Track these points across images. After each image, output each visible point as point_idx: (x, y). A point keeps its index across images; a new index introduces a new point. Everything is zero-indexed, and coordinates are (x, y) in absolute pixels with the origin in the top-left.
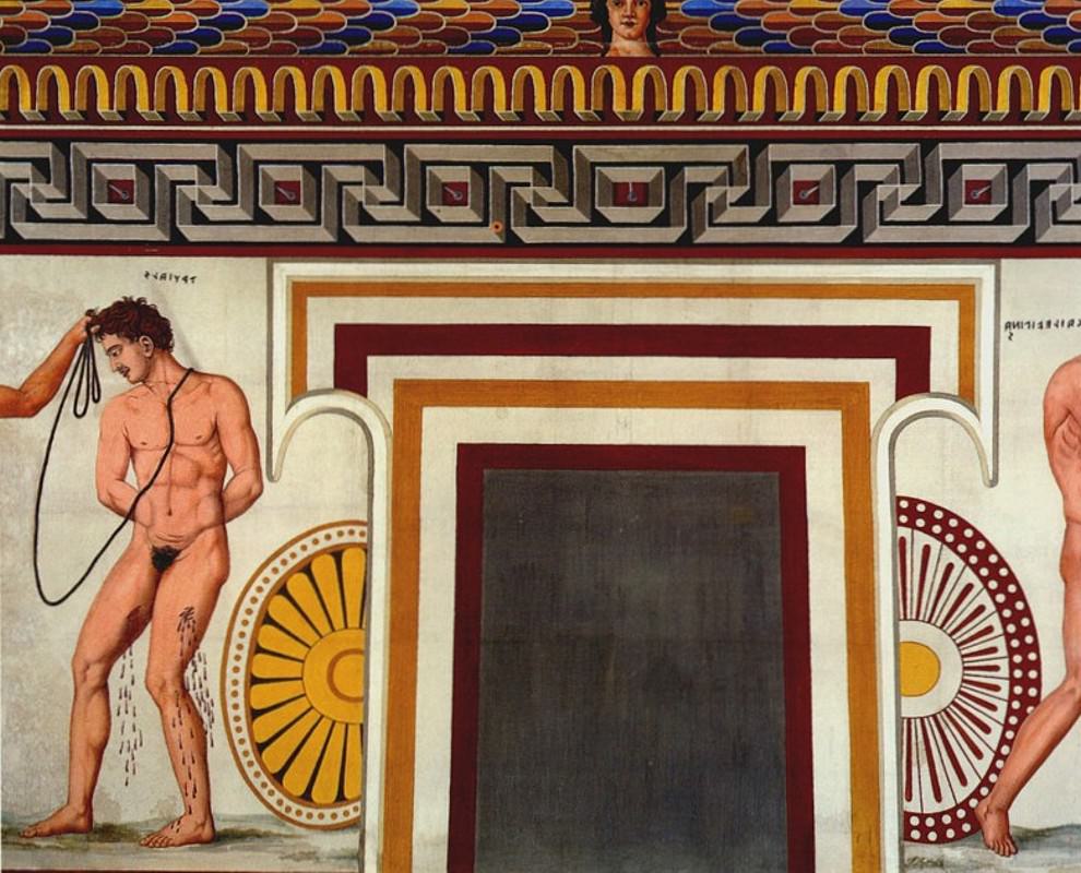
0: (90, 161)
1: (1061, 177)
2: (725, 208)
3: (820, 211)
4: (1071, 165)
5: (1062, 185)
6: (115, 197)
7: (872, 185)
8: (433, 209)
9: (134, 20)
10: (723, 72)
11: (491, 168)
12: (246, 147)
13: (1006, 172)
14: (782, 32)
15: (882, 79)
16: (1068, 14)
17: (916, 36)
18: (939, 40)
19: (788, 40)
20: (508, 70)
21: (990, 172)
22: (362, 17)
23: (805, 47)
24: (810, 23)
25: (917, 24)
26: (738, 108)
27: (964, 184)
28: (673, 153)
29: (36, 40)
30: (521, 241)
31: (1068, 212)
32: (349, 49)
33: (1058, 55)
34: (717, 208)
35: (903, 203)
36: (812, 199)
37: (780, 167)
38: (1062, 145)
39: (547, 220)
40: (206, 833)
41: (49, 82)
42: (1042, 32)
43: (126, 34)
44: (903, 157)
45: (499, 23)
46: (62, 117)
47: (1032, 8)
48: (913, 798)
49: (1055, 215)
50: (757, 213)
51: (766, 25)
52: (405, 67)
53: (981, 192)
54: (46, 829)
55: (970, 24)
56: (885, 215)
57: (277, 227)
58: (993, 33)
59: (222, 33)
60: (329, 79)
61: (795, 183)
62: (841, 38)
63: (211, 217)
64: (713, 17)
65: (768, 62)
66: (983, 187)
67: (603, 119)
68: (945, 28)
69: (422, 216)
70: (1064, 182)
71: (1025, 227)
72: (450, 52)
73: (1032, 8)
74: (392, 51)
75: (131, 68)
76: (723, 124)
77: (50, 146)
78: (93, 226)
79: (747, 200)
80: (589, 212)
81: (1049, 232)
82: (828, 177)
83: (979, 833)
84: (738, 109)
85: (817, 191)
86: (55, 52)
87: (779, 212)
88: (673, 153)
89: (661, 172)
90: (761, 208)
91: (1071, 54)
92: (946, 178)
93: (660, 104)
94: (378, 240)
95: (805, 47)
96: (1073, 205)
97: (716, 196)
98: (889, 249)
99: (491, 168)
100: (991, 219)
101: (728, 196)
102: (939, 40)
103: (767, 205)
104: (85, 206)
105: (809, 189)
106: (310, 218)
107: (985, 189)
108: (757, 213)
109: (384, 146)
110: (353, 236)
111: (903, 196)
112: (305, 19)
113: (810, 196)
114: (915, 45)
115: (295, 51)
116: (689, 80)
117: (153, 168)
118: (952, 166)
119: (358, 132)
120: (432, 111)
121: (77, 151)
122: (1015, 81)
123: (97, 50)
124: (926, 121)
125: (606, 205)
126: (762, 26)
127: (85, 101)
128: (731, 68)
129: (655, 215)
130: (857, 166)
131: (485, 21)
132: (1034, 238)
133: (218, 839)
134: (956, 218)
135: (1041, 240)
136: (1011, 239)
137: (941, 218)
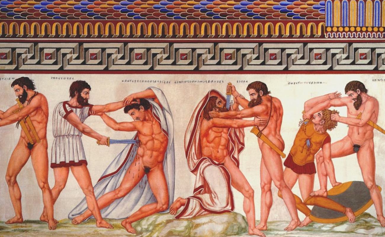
1: (250, 53)
2: (252, 61)
3: (97, 62)
4: (73, 49)
5: (115, 55)
6: (95, 58)
7: (156, 54)
10: (172, 24)
13: (56, 51)
14: (179, 14)
15: (12, 25)
16: (133, 9)
17: (253, 15)
18: (153, 15)
19: (73, 15)
21: (142, 51)
23: (210, 17)
24: (185, 11)
25: (214, 11)
26: (272, 34)
27: (90, 55)
29: (3, 13)
31: (44, 62)
33: (10, 19)
34: (24, 60)
35: (164, 59)
37: (42, 49)
38: (286, 44)
40: (265, 228)
42: (206, 14)
44: (253, 47)
47: (162, 7)
49: (204, 63)
50: (81, 61)
51: (254, 12)
53: (185, 57)
54: (11, 222)
55: (227, 12)
56: (160, 62)
58: (233, 14)
61: (181, 54)
62: (100, 15)
64: (121, 9)
65: (120, 21)
66: (4, 55)
68: (168, 13)
70: (206, 54)
71: (196, 66)
73: (162, 7)
76: (98, 38)
79: (78, 58)
81: (22, 67)
82: (369, 52)
84: (282, 34)
85: (187, 56)
87: (177, 62)
89: (100, 51)
90: (81, 60)
91: (293, 20)
92: (310, 52)
93: (293, 33)
94: (31, 69)
95: (210, 17)
96: (28, 60)
97: (339, 57)
98: (360, 71)
100: (259, 64)
101: (298, 57)
102: (153, 15)
103: (190, 59)
105: (94, 55)
107: (186, 56)
108: (81, 61)
111: (74, 57)
113: (274, 58)
114: (128, 13)
116: (131, 26)
118: (132, 50)
119: (357, 40)
122: (301, 27)
124: (215, 37)
126: (53, 12)
128: (153, 23)
129: (82, 62)
130: (90, 49)
132: (108, 69)
133: (22, 222)
134: (42, 63)
135: (155, 69)
136: (57, 69)
137: (263, 64)
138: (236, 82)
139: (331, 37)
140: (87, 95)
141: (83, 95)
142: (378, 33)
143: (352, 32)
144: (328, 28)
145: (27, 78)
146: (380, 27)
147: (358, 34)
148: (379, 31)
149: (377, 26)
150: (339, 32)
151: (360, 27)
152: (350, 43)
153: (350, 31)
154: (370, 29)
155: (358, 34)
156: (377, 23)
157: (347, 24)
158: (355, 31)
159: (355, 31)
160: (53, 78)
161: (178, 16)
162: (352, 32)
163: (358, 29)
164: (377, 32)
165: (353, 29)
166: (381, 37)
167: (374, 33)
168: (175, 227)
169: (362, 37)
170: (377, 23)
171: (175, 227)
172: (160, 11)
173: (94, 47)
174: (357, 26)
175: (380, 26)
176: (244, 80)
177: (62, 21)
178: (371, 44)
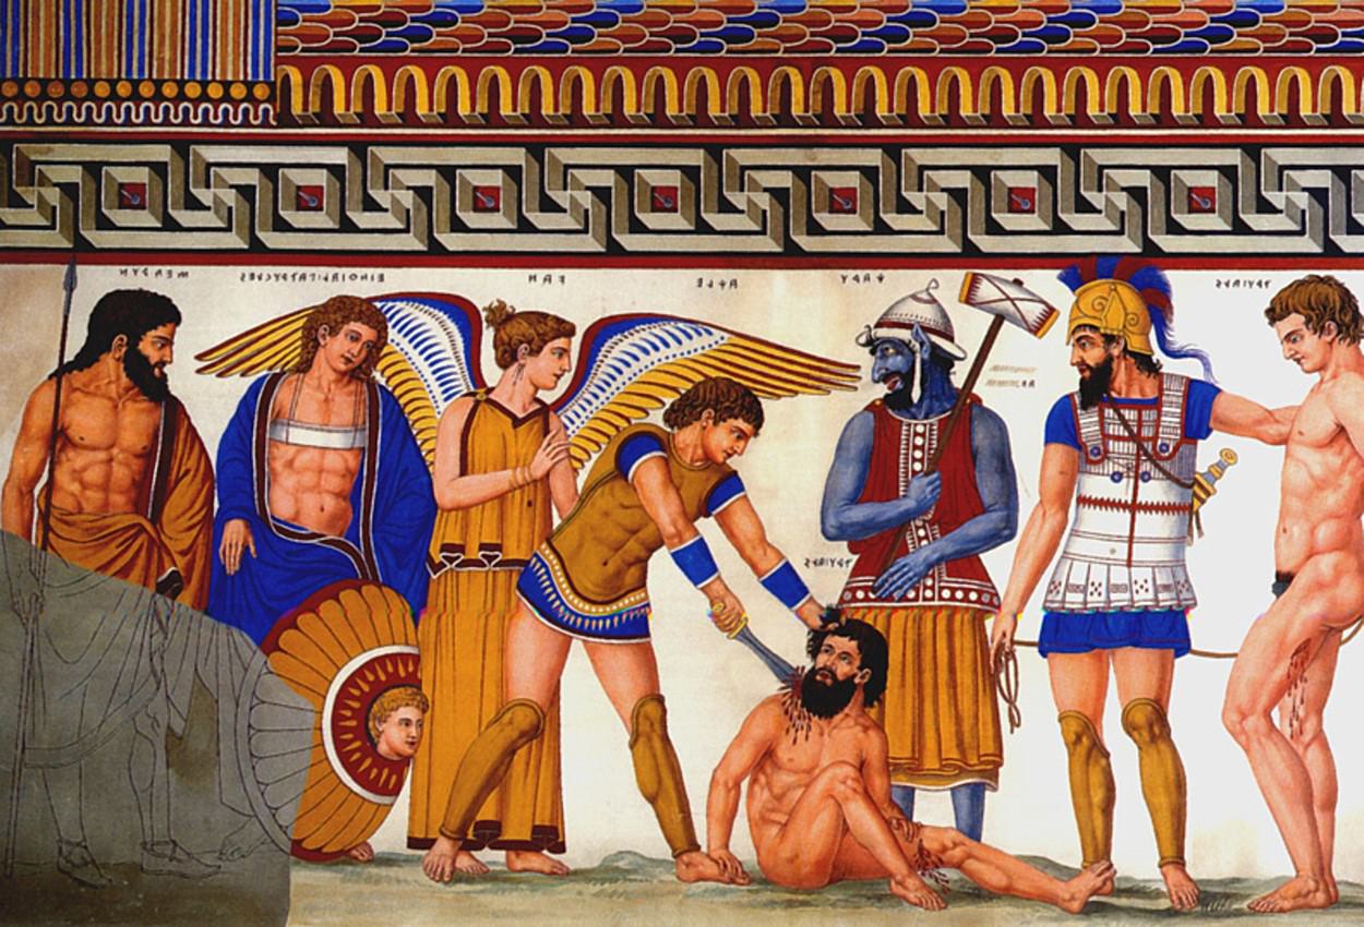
0: (1282, 168)
6: (1015, 206)
8: (1064, 217)
9: (1132, 18)
11: (813, 173)
12: (1270, 151)
20: (1059, 71)
22: (375, 14)
28: (796, 157)
30: (800, 248)
32: (887, 47)
36: (836, 206)
38: (851, 151)
39: (718, 228)
41: (1120, 86)
43: (967, 32)
45: (889, 20)
46: (1301, 119)
48: (402, 793)
52: (615, 68)
57: (539, 235)
59: (1071, 31)
60: (1039, 82)
63: (471, 225)
67: (612, 122)
69: (1234, 225)
72: (1049, 52)
74: (1257, 50)
75: (1336, 68)
77: (1057, 151)
78: (1242, 238)
80: (161, 216)
83: (966, 830)
86: (728, 51)
88: (796, 157)
99: (813, 173)
104: (693, 217)
106: (935, 228)
109: (169, 147)
110: (1161, 245)
112: (679, 16)
114: (1017, 41)
115: (406, 49)
117: (1350, 175)
119: (64, 133)
120: (768, 114)
121: (197, 155)
123: (297, 47)
125: (1182, 212)
127: (1030, 104)
131: (715, 19)
138: (696, 284)
139: (56, 119)
140: (167, 350)
141: (148, 347)
142: (66, 105)
143: (236, 103)
144: (51, 85)
145: (1330, 278)
146: (209, 82)
147: (141, 110)
148: (204, 97)
149: (198, 77)
150: (209, 100)
151: (154, 81)
152: (181, 145)
153: (227, 97)
154: (169, 90)
155: (141, 110)
156: (116, 69)
157: (79, 70)
158: (114, 96)
159: (250, 98)
160: (1223, 286)
161: (943, 46)
162: (236, 103)
163: (123, 89)
164: (60, 101)
165: (238, 92)
166: (193, 121)
167: (186, 104)
168: (652, 725)
169: (160, 120)
170: (218, 71)
171: (652, 725)
172: (1179, 34)
173: (1021, 172)
174: (120, 79)
175: (210, 77)
176: (276, 284)
177: (5, 55)
178: (1323, 151)
